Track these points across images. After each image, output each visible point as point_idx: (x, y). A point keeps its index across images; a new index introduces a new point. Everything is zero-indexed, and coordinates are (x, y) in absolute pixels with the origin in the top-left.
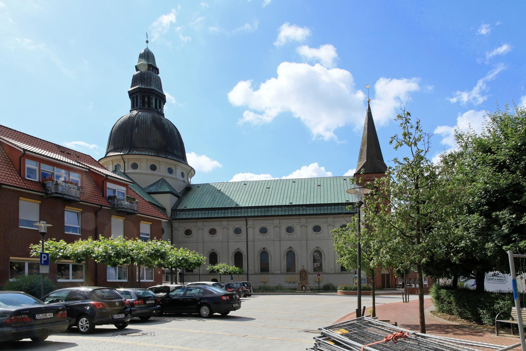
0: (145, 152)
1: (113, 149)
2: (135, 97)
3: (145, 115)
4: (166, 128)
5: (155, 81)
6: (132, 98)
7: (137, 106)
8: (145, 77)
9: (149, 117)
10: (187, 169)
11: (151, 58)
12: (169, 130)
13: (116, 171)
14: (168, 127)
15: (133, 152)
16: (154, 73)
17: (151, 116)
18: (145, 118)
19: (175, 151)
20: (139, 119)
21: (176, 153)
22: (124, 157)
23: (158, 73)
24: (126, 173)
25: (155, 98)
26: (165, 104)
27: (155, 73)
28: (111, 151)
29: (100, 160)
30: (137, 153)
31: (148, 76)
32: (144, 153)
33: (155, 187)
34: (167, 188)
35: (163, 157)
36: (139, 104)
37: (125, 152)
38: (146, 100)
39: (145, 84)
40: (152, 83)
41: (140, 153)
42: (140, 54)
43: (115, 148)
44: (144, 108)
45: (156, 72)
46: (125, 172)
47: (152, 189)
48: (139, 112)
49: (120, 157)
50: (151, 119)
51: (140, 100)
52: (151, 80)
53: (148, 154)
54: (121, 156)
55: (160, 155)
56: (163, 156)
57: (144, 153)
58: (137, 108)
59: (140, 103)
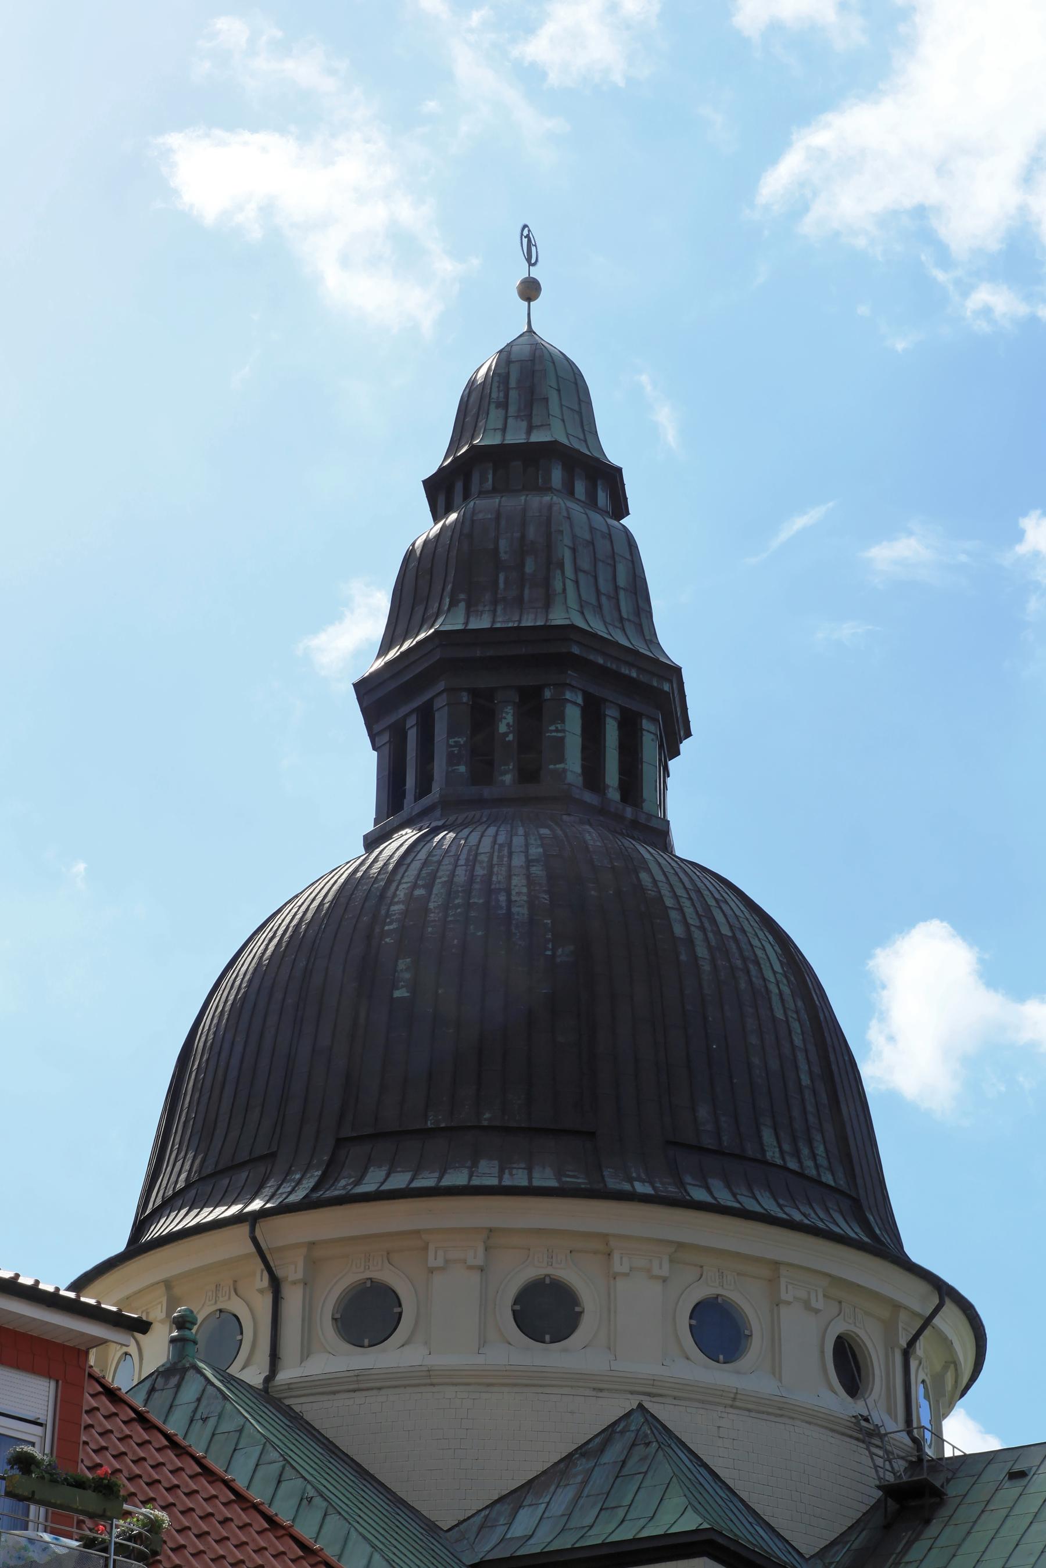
0: (475, 1164)
1: (189, 1185)
2: (412, 721)
3: (487, 842)
4: (679, 930)
5: (585, 564)
6: (385, 738)
7: (424, 787)
8: (496, 550)
9: (518, 861)
10: (896, 1307)
11: (553, 397)
12: (702, 951)
13: (184, 1371)
14: (693, 921)
15: (358, 1182)
16: (576, 510)
17: (536, 851)
18: (480, 871)
19: (768, 1136)
20: (429, 887)
21: (773, 1154)
22: (273, 1232)
23: (620, 508)
24: (289, 1387)
25: (587, 696)
26: (685, 746)
27: (592, 502)
28: (168, 1205)
29: (80, 1284)
30: (399, 1181)
31: (523, 537)
32: (457, 1178)
33: (562, 1499)
34: (676, 1501)
35: (645, 1199)
36: (439, 767)
37: (286, 1188)
38: (502, 728)
39: (495, 602)
40: (558, 585)
41: (427, 1181)
42: (472, 383)
43: (209, 1170)
44: (487, 792)
45: (603, 498)
46: (284, 1376)
47: (524, 1522)
48: (435, 831)
49: (238, 1240)
50: (537, 870)
51: (452, 732)
52: (551, 563)
53: (494, 1181)
54: (244, 1229)
55: (613, 1183)
56: (641, 1188)
57: (457, 1178)
58: (426, 801)
59: (453, 759)
